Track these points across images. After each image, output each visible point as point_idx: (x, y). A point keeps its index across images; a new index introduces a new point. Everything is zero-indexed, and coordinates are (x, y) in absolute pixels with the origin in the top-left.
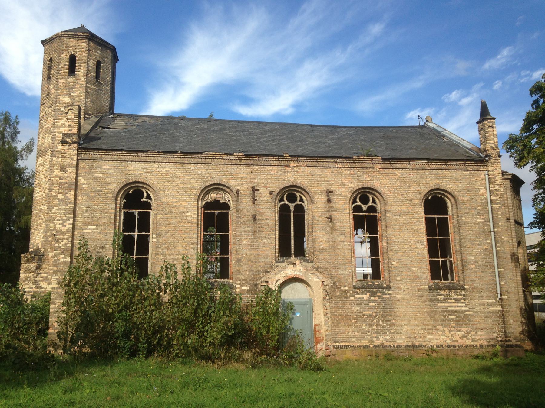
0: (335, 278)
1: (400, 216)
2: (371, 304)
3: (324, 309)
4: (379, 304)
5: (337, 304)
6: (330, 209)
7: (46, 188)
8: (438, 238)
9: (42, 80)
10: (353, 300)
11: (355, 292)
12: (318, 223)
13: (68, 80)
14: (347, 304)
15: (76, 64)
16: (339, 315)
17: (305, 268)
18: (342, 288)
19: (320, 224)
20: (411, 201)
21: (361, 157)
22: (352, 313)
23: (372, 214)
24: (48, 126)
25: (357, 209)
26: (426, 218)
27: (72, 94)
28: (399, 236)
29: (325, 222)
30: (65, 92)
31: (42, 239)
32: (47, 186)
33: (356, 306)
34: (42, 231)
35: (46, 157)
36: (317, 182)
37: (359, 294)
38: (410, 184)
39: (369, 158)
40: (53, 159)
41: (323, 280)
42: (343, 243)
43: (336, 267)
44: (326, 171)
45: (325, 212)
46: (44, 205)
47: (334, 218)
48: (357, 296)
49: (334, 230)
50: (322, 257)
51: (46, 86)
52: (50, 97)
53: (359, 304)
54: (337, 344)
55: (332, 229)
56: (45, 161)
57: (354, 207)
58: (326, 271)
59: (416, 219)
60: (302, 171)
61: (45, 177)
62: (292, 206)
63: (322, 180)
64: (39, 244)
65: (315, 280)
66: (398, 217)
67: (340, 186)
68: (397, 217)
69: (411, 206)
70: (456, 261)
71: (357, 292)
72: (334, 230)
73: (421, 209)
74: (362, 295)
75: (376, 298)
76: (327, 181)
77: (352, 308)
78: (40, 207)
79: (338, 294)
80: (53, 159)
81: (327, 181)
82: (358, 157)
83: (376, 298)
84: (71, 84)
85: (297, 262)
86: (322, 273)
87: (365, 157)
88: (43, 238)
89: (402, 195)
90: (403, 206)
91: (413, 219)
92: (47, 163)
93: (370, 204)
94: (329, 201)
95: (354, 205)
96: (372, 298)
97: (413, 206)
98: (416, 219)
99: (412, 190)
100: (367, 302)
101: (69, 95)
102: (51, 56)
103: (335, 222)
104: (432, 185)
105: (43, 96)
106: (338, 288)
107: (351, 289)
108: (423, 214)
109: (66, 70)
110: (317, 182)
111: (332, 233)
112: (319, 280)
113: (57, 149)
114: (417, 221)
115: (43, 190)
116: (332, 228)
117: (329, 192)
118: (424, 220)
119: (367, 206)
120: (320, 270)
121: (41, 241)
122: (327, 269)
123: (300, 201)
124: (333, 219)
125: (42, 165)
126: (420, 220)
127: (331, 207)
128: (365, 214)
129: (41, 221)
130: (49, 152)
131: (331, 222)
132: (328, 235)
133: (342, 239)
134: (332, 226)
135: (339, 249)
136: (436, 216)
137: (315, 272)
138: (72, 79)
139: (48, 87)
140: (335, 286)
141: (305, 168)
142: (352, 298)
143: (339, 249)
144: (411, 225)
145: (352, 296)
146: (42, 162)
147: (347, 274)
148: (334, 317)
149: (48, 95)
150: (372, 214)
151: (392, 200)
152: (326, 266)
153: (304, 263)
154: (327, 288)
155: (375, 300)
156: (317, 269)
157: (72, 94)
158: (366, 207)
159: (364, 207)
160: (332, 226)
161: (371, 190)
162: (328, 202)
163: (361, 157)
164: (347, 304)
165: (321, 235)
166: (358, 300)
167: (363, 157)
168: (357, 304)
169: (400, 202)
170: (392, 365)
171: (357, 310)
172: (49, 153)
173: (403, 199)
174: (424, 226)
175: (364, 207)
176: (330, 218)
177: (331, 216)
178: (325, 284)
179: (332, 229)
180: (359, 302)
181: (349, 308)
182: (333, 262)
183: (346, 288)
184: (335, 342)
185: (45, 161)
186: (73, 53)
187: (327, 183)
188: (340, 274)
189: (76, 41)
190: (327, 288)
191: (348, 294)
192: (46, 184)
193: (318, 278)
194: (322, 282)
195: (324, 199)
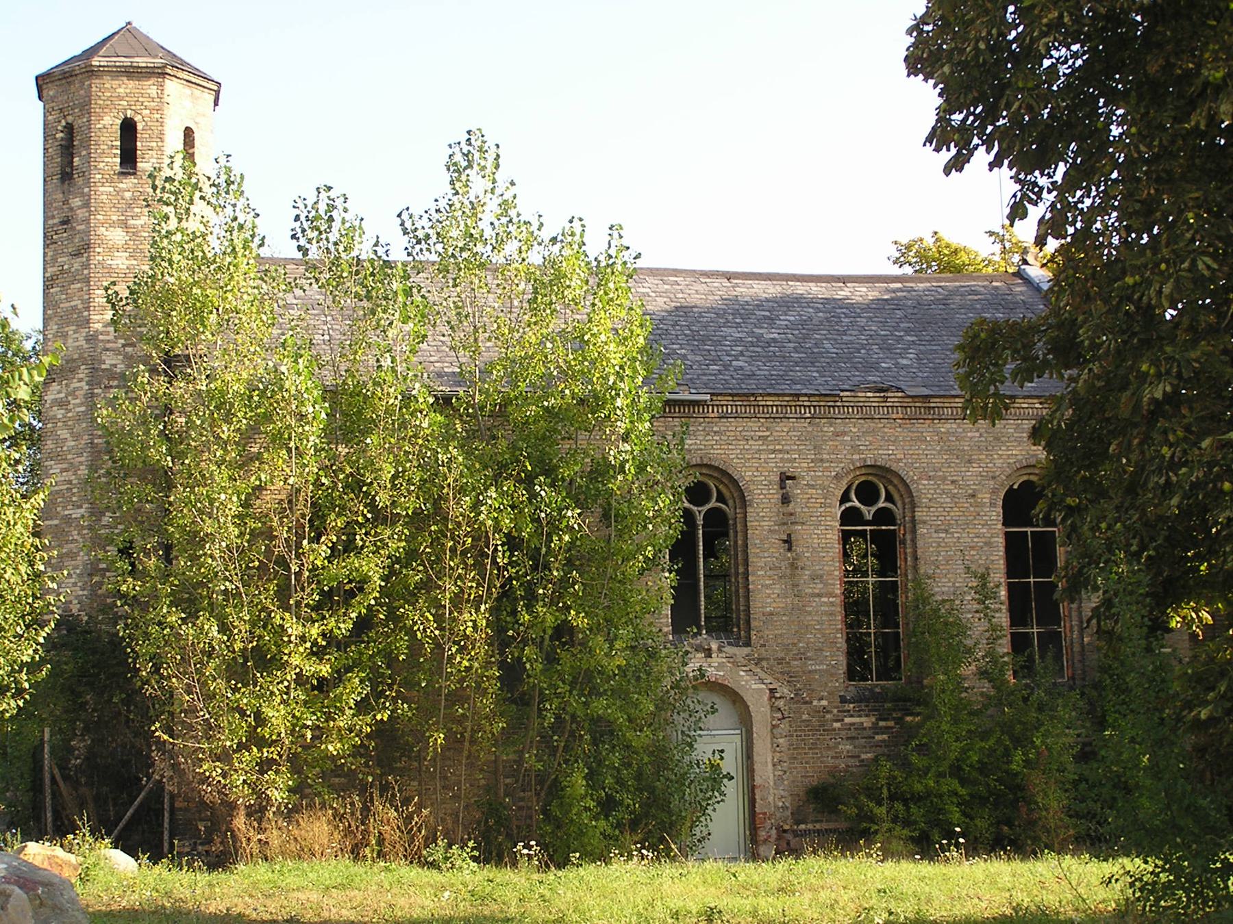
0: (798, 682)
1: (946, 531)
2: (878, 737)
3: (775, 751)
4: (896, 737)
5: (803, 740)
6: (788, 519)
7: (81, 463)
8: (1032, 580)
9: (45, 180)
10: (839, 729)
11: (844, 711)
12: (761, 555)
13: (121, 185)
14: (824, 739)
15: (139, 144)
16: (806, 763)
17: (731, 660)
18: (815, 703)
19: (766, 555)
20: (973, 496)
21: (860, 394)
22: (837, 758)
23: (883, 528)
24: (73, 304)
25: (850, 517)
26: (1007, 534)
27: (131, 222)
28: (944, 580)
29: (777, 549)
30: (114, 218)
31: (81, 593)
32: (82, 459)
33: (845, 742)
34: (78, 571)
35: (73, 386)
36: (757, 456)
37: (852, 716)
38: (971, 455)
39: (878, 395)
40: (96, 391)
41: (771, 687)
42: (817, 599)
43: (802, 656)
44: (777, 429)
45: (777, 527)
46: (81, 507)
47: (797, 540)
48: (847, 720)
49: (797, 568)
50: (769, 633)
51: (60, 196)
52: (73, 228)
53: (853, 738)
54: (803, 827)
55: (793, 566)
56: (73, 393)
57: (843, 513)
58: (779, 664)
59: (983, 540)
60: (722, 428)
61: (76, 437)
62: (700, 512)
63: (768, 450)
64: (71, 602)
65: (753, 686)
66: (944, 535)
67: (812, 465)
68: (941, 535)
69: (972, 509)
70: (1068, 634)
71: (849, 711)
72: (797, 568)
73: (997, 514)
74: (860, 716)
75: (891, 724)
76: (780, 451)
77: (836, 747)
78: (67, 512)
79: (805, 717)
80: (96, 391)
81: (780, 451)
82: (853, 394)
83: (891, 724)
84: (128, 195)
85: (714, 646)
86: (770, 670)
87: (869, 394)
88: (83, 590)
89: (953, 482)
90: (955, 509)
91: (975, 540)
92: (78, 401)
93: (881, 504)
94: (786, 500)
95: (843, 508)
96: (882, 724)
97: (977, 509)
98: (983, 540)
99: (975, 469)
100: (870, 733)
101: (125, 225)
102: (70, 119)
103: (799, 550)
104: (1020, 457)
105: (50, 222)
106: (806, 703)
107: (835, 704)
108: (1000, 526)
109: (114, 160)
110: (757, 456)
111: (793, 576)
112: (764, 686)
113: (103, 367)
114: (986, 543)
115: (73, 468)
116: (792, 565)
117: (785, 478)
118: (1000, 541)
119: (873, 509)
120: (764, 664)
121: (77, 597)
122: (780, 661)
123: (717, 501)
124: (794, 544)
125: (62, 404)
126: (993, 540)
127: (791, 514)
128: (868, 528)
129: (72, 545)
130: (83, 372)
131: (790, 549)
132: (783, 581)
133: (817, 591)
134: (794, 559)
135: (810, 613)
136: (1029, 530)
137: (752, 667)
138: (130, 182)
139: (66, 202)
140: (798, 699)
141: (730, 422)
142: (837, 725)
143: (810, 613)
144: (972, 553)
145: (837, 721)
146: (62, 395)
147: (826, 671)
148: (795, 768)
149: (65, 222)
150: (883, 528)
151: (930, 496)
152: (780, 655)
153: (730, 650)
154: (781, 703)
155: (887, 728)
156: (758, 662)
157: (131, 222)
158: (872, 513)
159: (868, 512)
160: (794, 559)
161: (884, 472)
162: (783, 503)
163: (860, 394)
164: (824, 739)
165: (767, 582)
166: (850, 729)
167: (863, 394)
168: (848, 738)
169: (948, 500)
170: (73, 692)
171: (848, 752)
172: (81, 376)
173: (956, 491)
174: (1001, 553)
175: (868, 512)
176: (788, 542)
177: (789, 535)
178: (778, 695)
179: (793, 566)
180: (853, 733)
181: (829, 748)
182: (795, 644)
183: (824, 703)
184: (798, 824)
185: (73, 393)
186: (129, 114)
187: (781, 456)
188: (810, 672)
189: (132, 84)
190: (781, 703)
191: (828, 716)
192: (80, 455)
193: (762, 681)
194: (771, 690)
195: (775, 494)
